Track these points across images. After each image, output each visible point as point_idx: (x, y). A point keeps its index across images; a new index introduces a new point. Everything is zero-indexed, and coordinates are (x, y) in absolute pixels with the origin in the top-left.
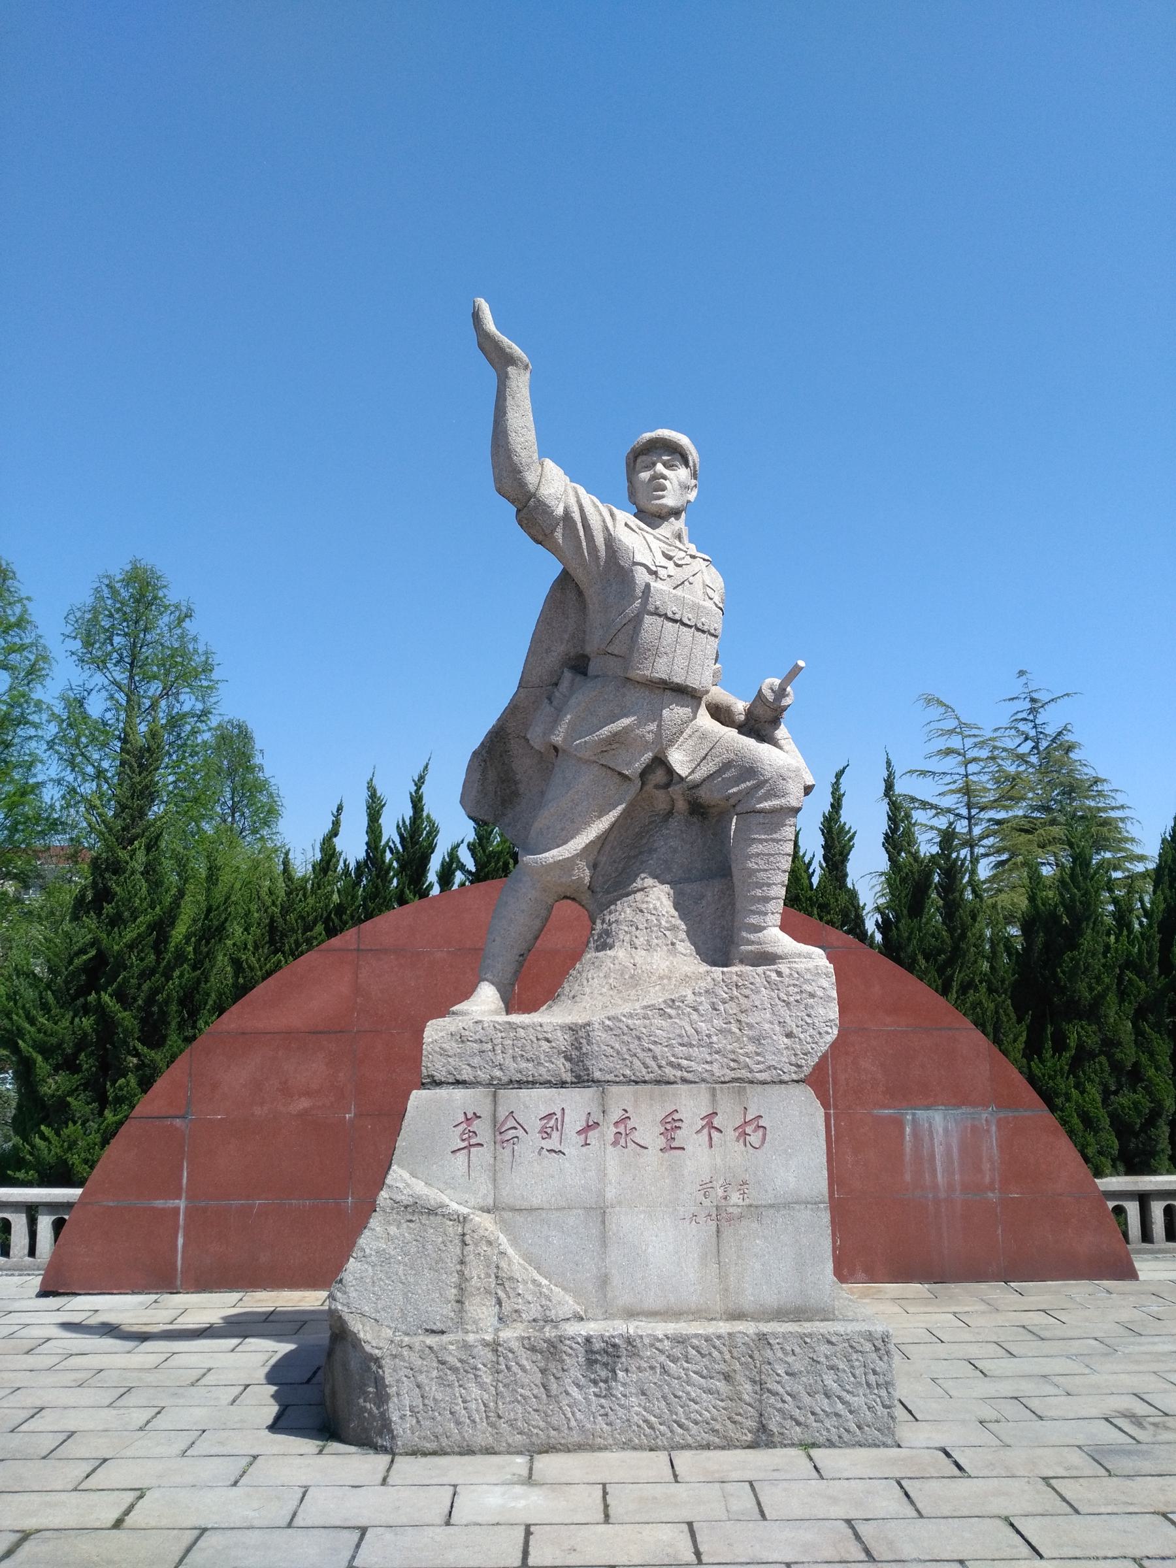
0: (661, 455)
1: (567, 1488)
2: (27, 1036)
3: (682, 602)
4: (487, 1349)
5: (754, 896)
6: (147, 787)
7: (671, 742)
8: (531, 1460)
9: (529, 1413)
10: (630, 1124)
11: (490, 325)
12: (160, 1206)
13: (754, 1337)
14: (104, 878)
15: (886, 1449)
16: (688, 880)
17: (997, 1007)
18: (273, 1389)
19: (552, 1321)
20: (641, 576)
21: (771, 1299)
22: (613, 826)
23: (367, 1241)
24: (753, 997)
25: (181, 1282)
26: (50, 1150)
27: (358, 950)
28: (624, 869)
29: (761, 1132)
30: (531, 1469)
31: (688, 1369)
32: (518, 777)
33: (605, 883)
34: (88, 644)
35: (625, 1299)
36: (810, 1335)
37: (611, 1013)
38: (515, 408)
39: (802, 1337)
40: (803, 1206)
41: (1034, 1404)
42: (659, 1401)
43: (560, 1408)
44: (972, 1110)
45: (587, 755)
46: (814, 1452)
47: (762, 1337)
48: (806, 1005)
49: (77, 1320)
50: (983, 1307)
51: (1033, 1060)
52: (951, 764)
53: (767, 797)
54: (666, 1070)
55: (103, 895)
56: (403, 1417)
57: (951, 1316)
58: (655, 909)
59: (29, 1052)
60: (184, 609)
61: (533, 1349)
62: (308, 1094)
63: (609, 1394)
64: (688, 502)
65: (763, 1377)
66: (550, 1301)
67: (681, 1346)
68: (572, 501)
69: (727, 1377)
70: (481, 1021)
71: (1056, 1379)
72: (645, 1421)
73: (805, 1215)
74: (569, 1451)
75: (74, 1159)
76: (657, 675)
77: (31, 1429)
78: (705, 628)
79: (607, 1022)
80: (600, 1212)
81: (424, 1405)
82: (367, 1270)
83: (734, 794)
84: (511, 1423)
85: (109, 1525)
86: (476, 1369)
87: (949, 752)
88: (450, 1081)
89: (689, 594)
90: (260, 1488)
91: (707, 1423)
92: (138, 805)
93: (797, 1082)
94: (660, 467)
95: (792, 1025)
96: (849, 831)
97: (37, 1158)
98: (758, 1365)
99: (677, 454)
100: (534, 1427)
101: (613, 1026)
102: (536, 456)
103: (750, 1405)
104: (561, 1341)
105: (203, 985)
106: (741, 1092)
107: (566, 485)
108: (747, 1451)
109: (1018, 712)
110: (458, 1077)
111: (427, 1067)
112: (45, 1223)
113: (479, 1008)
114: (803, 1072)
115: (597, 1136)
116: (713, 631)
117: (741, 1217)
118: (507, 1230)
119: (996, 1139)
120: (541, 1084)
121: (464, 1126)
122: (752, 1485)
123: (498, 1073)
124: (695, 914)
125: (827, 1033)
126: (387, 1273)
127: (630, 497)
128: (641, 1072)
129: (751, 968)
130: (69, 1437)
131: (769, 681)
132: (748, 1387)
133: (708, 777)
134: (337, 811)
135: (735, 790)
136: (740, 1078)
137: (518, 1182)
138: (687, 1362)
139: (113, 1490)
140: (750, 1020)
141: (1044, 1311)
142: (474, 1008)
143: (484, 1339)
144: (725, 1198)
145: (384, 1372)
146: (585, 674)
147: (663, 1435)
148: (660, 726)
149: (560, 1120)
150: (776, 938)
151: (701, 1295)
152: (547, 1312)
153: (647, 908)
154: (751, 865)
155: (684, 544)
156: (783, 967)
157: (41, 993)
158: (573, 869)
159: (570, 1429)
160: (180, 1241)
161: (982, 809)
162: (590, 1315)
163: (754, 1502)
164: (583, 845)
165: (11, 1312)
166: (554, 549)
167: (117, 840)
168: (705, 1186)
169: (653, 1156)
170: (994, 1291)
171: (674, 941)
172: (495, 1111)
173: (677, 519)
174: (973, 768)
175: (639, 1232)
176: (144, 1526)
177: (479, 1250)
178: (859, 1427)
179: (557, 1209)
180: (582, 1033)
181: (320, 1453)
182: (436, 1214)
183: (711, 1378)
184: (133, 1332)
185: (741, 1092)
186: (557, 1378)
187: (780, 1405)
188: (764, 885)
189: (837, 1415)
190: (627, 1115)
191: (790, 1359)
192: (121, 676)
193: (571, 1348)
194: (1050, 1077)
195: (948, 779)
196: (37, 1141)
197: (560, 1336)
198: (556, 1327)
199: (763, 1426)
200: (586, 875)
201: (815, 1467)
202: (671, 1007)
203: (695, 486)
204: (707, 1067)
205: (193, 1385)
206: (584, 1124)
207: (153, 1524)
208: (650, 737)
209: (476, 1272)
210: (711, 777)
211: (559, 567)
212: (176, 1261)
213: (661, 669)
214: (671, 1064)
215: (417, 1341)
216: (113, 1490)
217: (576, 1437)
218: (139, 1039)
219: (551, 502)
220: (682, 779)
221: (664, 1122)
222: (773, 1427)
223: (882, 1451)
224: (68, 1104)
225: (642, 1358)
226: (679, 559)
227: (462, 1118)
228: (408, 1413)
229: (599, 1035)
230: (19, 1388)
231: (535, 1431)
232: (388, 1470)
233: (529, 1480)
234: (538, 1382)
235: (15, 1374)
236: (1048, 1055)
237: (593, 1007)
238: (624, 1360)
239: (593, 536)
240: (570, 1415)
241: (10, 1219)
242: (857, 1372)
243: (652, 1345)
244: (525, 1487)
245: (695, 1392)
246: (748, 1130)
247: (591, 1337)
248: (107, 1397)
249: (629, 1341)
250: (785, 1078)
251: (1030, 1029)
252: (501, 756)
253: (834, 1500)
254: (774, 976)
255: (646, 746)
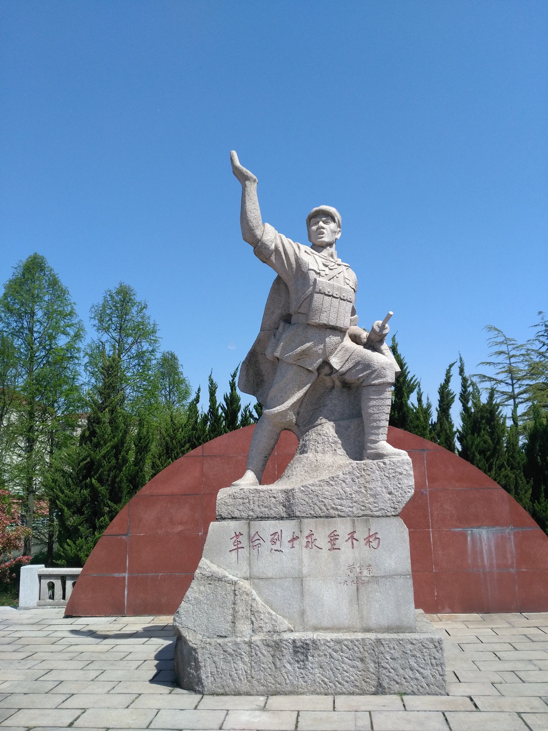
0: (322, 218)
1: (281, 712)
2: (60, 499)
3: (333, 287)
4: (246, 645)
5: (373, 426)
6: (111, 384)
7: (331, 354)
8: (267, 699)
9: (267, 676)
10: (314, 537)
11: (237, 163)
12: (117, 576)
13: (375, 640)
14: (93, 426)
15: (441, 696)
16: (342, 419)
17: (516, 476)
18: (157, 662)
19: (277, 632)
20: (312, 275)
21: (384, 622)
22: (305, 394)
23: (189, 593)
24: (372, 475)
25: (127, 611)
26: (71, 550)
27: (203, 456)
28: (312, 415)
29: (377, 541)
30: (266, 703)
31: (342, 656)
32: (263, 373)
33: (304, 422)
34: (101, 321)
35: (312, 621)
36: (402, 640)
37: (304, 484)
38: (250, 200)
39: (398, 640)
40: (399, 577)
41: (521, 675)
42: (329, 671)
43: (282, 674)
44: (501, 528)
45: (291, 361)
46: (405, 698)
47: (379, 641)
48: (398, 478)
49: (78, 629)
50: (507, 625)
51: (535, 502)
52: (502, 358)
53: (377, 378)
54: (331, 511)
55: (93, 433)
56: (207, 677)
57: (490, 630)
58: (326, 433)
59: (61, 506)
60: (143, 305)
61: (268, 645)
62: (181, 523)
63: (305, 668)
64: (336, 239)
65: (379, 660)
66: (276, 622)
67: (339, 645)
68: (279, 242)
69: (362, 660)
70: (243, 489)
71: (535, 662)
72: (323, 681)
73: (400, 581)
74: (286, 695)
75: (82, 555)
76: (322, 322)
77: (44, 679)
78: (345, 298)
79: (302, 488)
80: (300, 580)
81: (217, 671)
82: (190, 607)
83: (361, 377)
84: (258, 681)
85: (66, 725)
86: (241, 654)
87: (501, 353)
88: (229, 517)
89: (339, 283)
90: (138, 710)
91: (353, 682)
92: (107, 392)
93: (395, 516)
94: (321, 224)
95: (391, 488)
96: (452, 394)
97: (66, 554)
98: (377, 654)
99: (330, 217)
100: (269, 683)
101: (305, 490)
102: (261, 222)
103: (373, 674)
104: (281, 642)
105: (140, 473)
106: (367, 521)
107: (276, 235)
108: (372, 696)
109: (539, 332)
110: (233, 515)
111: (218, 511)
112: (69, 583)
113: (244, 483)
114: (397, 511)
115: (298, 543)
116: (349, 300)
117: (368, 582)
118: (256, 588)
119: (514, 542)
120: (272, 518)
121: (235, 538)
122: (370, 713)
123: (251, 513)
124: (345, 435)
125: (409, 492)
126: (199, 608)
127: (309, 239)
128: (318, 512)
129: (371, 461)
130: (60, 683)
131: (377, 322)
132: (372, 665)
133: (349, 369)
134: (198, 391)
135: (361, 375)
136: (366, 515)
137: (261, 565)
138: (342, 652)
139: (73, 709)
140: (370, 486)
141: (537, 627)
142: (242, 483)
143: (245, 640)
144: (361, 573)
145: (198, 655)
146: (290, 323)
147: (331, 688)
148: (325, 346)
149: (280, 535)
150: (384, 446)
151: (350, 620)
152: (275, 627)
153: (322, 433)
154: (370, 411)
155: (334, 259)
156: (386, 460)
157: (66, 479)
158: (287, 416)
159: (286, 684)
160: (126, 592)
161: (519, 380)
162: (296, 629)
163: (369, 721)
164: (291, 404)
165: (50, 625)
166: (271, 265)
167: (98, 408)
168: (350, 567)
169: (325, 553)
170: (514, 617)
171: (336, 448)
172: (249, 531)
173: (331, 247)
174: (513, 360)
175: (319, 589)
176: (82, 726)
177: (242, 598)
178: (428, 685)
179: (279, 578)
180: (290, 494)
181: (170, 693)
182: (222, 581)
183: (354, 660)
184: (103, 635)
185: (367, 521)
186: (279, 660)
187: (388, 674)
188: (377, 420)
189: (417, 679)
190: (312, 533)
191: (392, 651)
192: (115, 335)
193: (286, 645)
194: (544, 511)
195: (501, 366)
196: (66, 546)
197: (281, 639)
198: (279, 635)
199: (380, 684)
200: (294, 418)
201: (404, 705)
202: (332, 481)
203: (340, 231)
204: (350, 509)
205: (121, 660)
206: (292, 537)
207: (86, 725)
208: (320, 351)
209: (241, 608)
210: (350, 369)
211: (276, 275)
212: (124, 602)
213: (324, 319)
214: (333, 508)
215: (213, 641)
216: (73, 709)
217: (289, 688)
218: (109, 499)
219: (268, 243)
220: (337, 371)
221: (330, 536)
222: (385, 684)
223: (440, 697)
224: (79, 529)
225: (320, 650)
226: (331, 266)
227: (234, 535)
228: (210, 675)
229: (298, 494)
230: (44, 660)
231: (270, 685)
232: (199, 702)
233: (264, 709)
234: (271, 661)
235: (45, 653)
236: (542, 500)
237: (297, 481)
238: (311, 651)
239: (289, 258)
240: (286, 677)
241: (54, 582)
242: (426, 658)
243: (325, 644)
244: (261, 712)
245: (346, 667)
246: (371, 540)
247: (296, 640)
248: (81, 665)
249: (314, 642)
250: (389, 514)
251: (534, 488)
252: (255, 363)
253: (409, 721)
254: (382, 464)
255: (319, 356)
